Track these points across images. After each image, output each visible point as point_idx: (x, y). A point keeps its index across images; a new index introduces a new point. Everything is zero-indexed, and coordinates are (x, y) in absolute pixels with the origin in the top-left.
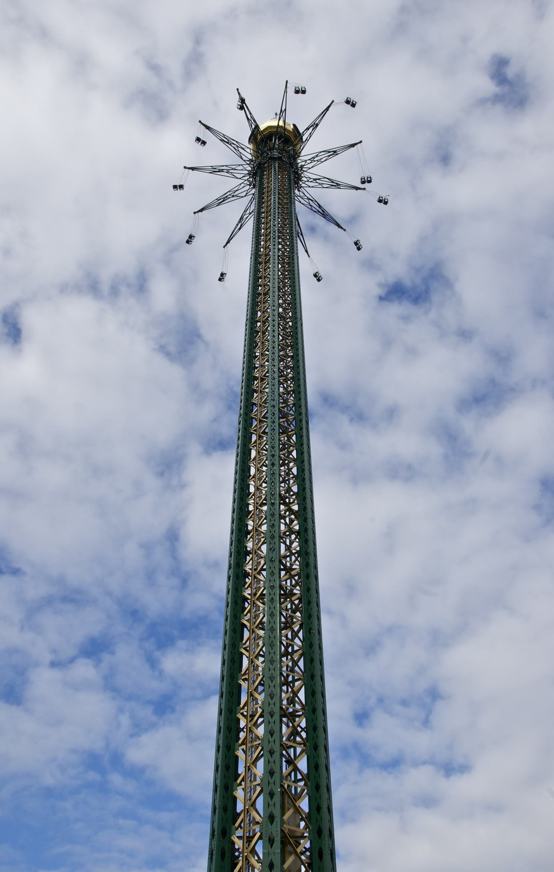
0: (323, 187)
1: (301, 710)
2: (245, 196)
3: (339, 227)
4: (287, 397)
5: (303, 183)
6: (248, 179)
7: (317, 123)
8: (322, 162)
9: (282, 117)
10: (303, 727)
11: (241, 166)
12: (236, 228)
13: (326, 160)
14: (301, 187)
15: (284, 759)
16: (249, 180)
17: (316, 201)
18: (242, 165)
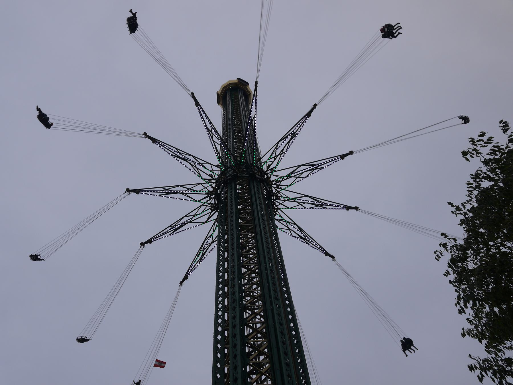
1: (262, 361)
2: (206, 222)
3: (326, 255)
4: (250, 291)
5: (280, 204)
6: (208, 201)
9: (300, 177)
10: (268, 383)
14: (278, 209)
15: (209, 205)
16: (209, 202)
17: (295, 224)
18: (211, 164)
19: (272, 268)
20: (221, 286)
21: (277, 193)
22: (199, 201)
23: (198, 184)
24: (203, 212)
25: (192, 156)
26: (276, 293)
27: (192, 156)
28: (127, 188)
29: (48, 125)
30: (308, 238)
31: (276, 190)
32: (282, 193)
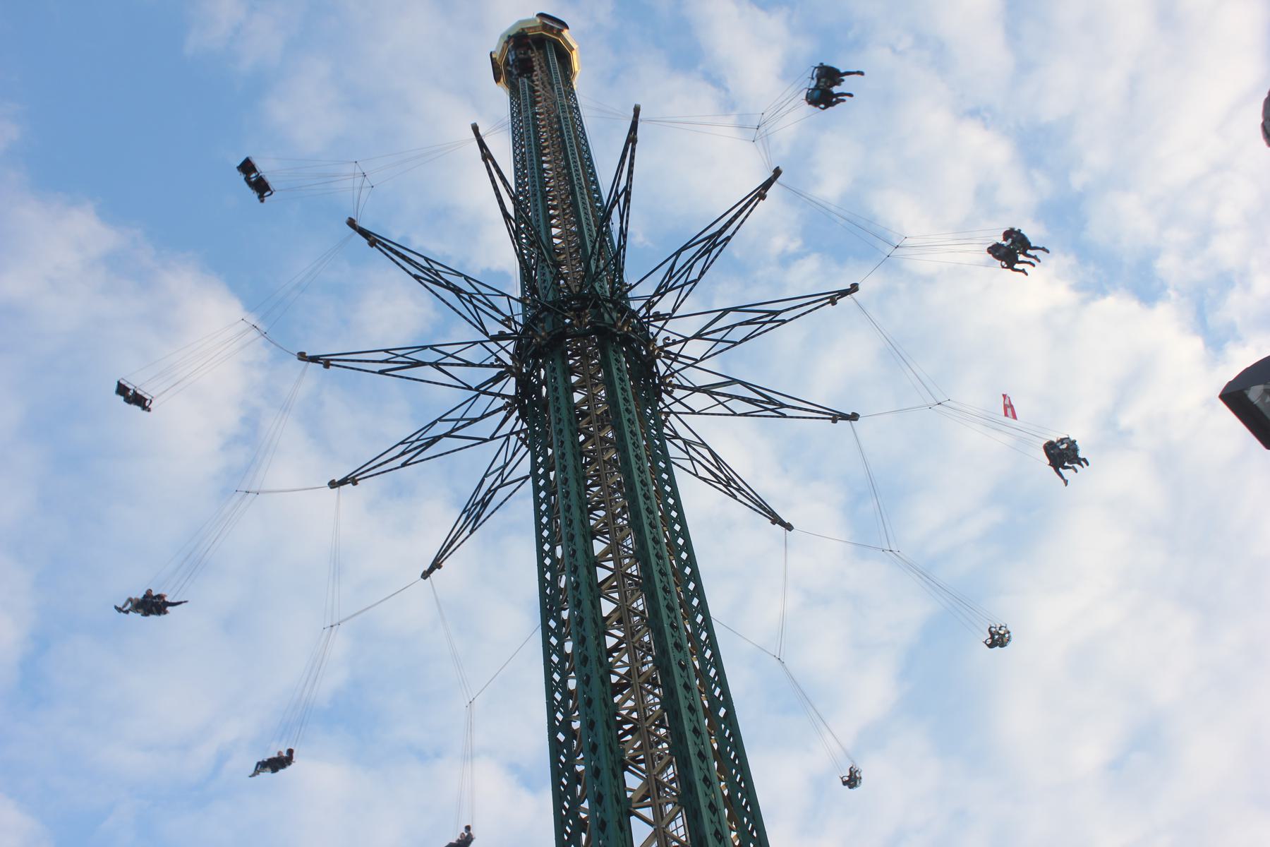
0: (735, 344)
7: (625, 189)
8: (696, 282)
11: (479, 344)
12: (504, 184)
13: (702, 273)
19: (644, 478)
20: (542, 494)
21: (669, 376)
22: (492, 438)
23: (475, 343)
24: (514, 454)
25: (463, 278)
26: (639, 461)
27: (463, 278)
28: (329, 481)
29: (122, 390)
30: (735, 483)
31: (669, 367)
32: (683, 377)
